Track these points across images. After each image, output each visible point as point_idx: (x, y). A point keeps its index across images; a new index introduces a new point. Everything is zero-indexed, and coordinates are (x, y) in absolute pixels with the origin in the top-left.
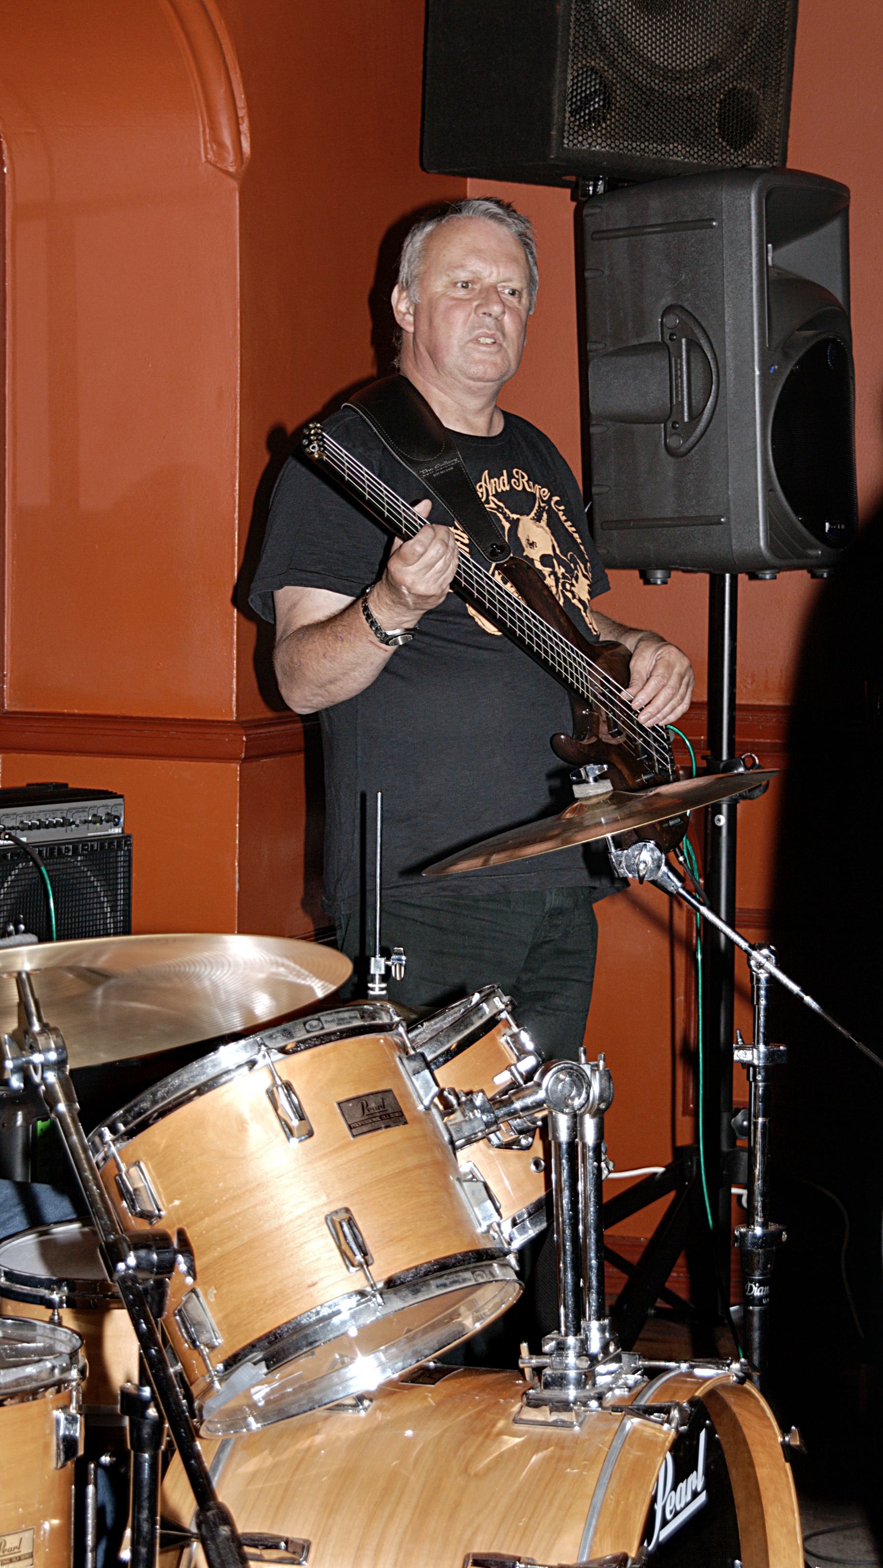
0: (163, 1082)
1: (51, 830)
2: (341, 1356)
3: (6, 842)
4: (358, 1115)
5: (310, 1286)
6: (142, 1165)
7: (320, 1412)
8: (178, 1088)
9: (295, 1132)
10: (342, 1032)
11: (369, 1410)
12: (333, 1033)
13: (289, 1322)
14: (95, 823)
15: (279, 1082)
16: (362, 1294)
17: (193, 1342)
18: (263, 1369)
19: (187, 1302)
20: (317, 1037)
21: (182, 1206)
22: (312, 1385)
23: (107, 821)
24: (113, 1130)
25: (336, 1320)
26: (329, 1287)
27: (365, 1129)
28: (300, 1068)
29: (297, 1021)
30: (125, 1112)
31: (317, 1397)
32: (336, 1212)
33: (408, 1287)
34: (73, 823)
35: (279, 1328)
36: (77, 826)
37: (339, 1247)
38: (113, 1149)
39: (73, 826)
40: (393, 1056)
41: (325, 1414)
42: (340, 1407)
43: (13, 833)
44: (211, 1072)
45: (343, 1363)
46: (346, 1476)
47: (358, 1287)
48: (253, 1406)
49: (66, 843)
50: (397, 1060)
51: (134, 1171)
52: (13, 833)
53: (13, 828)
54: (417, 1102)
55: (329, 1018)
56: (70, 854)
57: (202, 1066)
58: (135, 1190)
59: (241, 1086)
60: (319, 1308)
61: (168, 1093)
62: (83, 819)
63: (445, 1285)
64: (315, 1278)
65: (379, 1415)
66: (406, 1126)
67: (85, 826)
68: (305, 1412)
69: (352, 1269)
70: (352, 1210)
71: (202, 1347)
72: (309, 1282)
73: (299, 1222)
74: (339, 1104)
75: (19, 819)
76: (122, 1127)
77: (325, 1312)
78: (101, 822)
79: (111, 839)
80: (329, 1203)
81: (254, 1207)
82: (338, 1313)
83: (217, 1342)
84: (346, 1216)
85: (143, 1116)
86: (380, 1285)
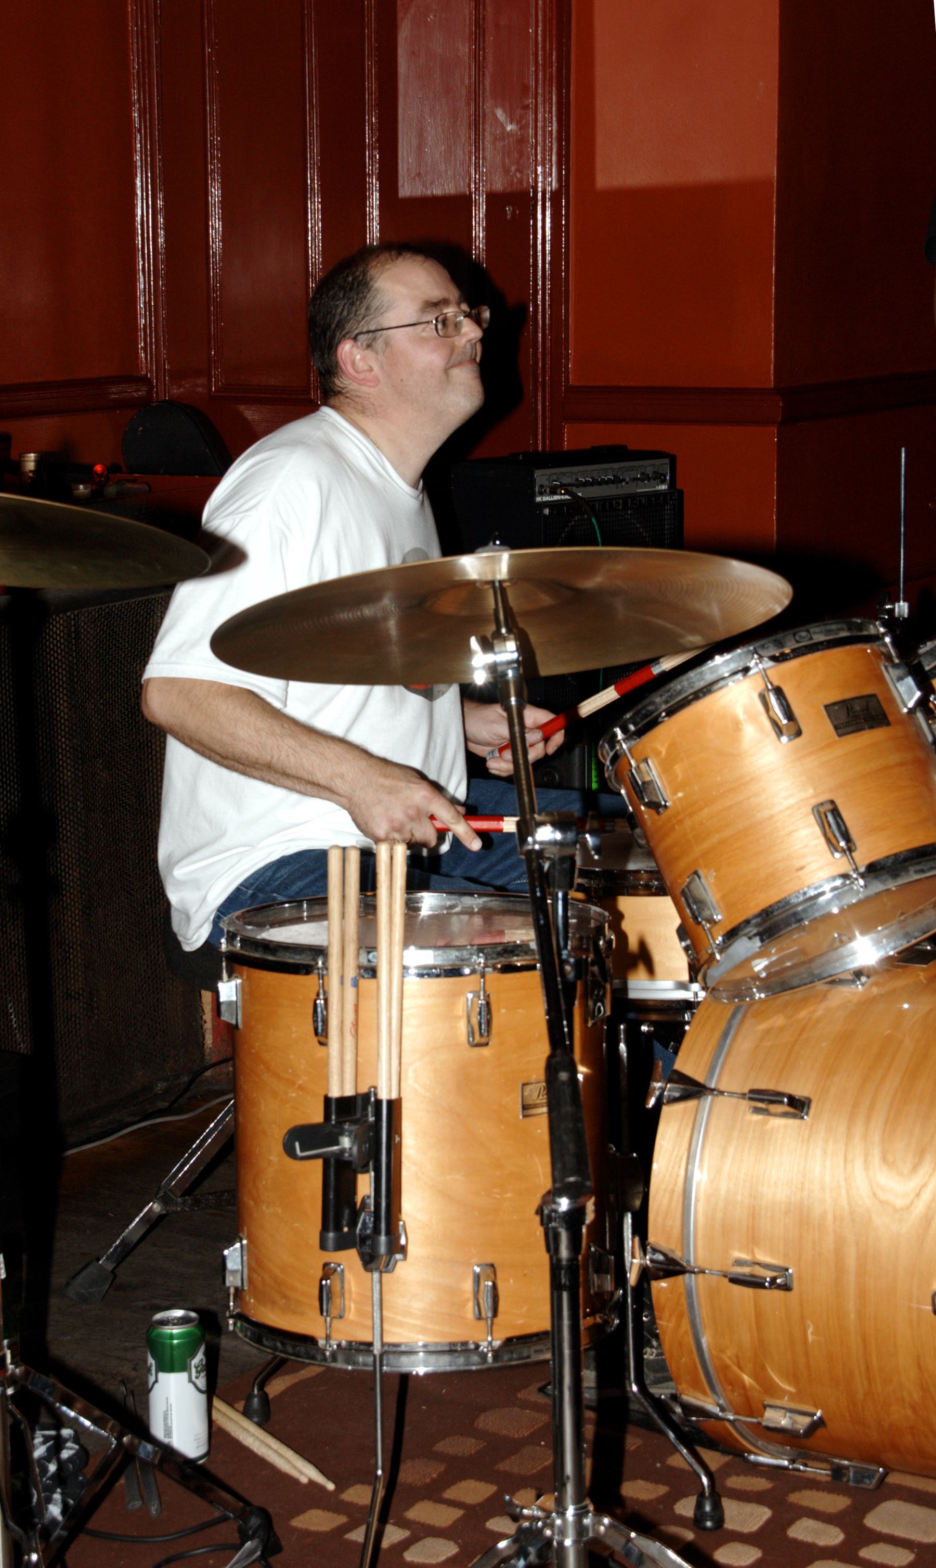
0: (667, 687)
1: (604, 486)
2: (840, 935)
3: (563, 497)
4: (843, 717)
5: (798, 870)
6: (650, 762)
7: (820, 986)
8: (680, 692)
9: (784, 730)
10: (828, 642)
11: (866, 986)
12: (821, 643)
13: (779, 902)
14: (643, 480)
15: (770, 687)
16: (845, 876)
17: (695, 918)
18: (757, 943)
19: (690, 883)
20: (805, 647)
21: (684, 797)
22: (811, 961)
23: (655, 479)
24: (625, 730)
25: (822, 899)
26: (815, 870)
27: (849, 729)
28: (786, 673)
29: (787, 633)
30: (635, 714)
31: (817, 972)
32: (822, 804)
33: (888, 872)
34: (624, 480)
35: (770, 906)
36: (627, 483)
37: (825, 835)
38: (624, 746)
39: (623, 483)
40: (878, 665)
41: (826, 987)
42: (841, 982)
43: (569, 488)
44: (709, 678)
45: (841, 941)
46: (844, 1040)
47: (842, 871)
48: (756, 977)
49: (616, 498)
50: (883, 668)
51: (643, 766)
52: (569, 488)
53: (569, 485)
54: (901, 705)
55: (817, 630)
56: (620, 507)
57: (701, 673)
58: (644, 783)
59: (738, 693)
60: (806, 889)
61: (670, 697)
62: (632, 476)
63: (923, 871)
64: (803, 862)
65: (875, 990)
66: (889, 728)
67: (634, 484)
68: (806, 984)
69: (837, 855)
70: (838, 802)
71: (704, 923)
72: (798, 866)
73: (788, 812)
74: (826, 707)
75: (574, 477)
76: (632, 728)
77: (812, 893)
78: (649, 479)
79: (658, 494)
80: (816, 796)
81: (748, 798)
82: (823, 894)
83: (718, 917)
84: (830, 807)
85: (649, 719)
86: (862, 870)
